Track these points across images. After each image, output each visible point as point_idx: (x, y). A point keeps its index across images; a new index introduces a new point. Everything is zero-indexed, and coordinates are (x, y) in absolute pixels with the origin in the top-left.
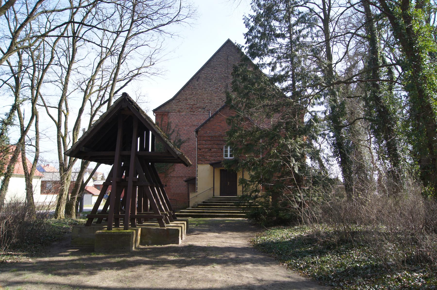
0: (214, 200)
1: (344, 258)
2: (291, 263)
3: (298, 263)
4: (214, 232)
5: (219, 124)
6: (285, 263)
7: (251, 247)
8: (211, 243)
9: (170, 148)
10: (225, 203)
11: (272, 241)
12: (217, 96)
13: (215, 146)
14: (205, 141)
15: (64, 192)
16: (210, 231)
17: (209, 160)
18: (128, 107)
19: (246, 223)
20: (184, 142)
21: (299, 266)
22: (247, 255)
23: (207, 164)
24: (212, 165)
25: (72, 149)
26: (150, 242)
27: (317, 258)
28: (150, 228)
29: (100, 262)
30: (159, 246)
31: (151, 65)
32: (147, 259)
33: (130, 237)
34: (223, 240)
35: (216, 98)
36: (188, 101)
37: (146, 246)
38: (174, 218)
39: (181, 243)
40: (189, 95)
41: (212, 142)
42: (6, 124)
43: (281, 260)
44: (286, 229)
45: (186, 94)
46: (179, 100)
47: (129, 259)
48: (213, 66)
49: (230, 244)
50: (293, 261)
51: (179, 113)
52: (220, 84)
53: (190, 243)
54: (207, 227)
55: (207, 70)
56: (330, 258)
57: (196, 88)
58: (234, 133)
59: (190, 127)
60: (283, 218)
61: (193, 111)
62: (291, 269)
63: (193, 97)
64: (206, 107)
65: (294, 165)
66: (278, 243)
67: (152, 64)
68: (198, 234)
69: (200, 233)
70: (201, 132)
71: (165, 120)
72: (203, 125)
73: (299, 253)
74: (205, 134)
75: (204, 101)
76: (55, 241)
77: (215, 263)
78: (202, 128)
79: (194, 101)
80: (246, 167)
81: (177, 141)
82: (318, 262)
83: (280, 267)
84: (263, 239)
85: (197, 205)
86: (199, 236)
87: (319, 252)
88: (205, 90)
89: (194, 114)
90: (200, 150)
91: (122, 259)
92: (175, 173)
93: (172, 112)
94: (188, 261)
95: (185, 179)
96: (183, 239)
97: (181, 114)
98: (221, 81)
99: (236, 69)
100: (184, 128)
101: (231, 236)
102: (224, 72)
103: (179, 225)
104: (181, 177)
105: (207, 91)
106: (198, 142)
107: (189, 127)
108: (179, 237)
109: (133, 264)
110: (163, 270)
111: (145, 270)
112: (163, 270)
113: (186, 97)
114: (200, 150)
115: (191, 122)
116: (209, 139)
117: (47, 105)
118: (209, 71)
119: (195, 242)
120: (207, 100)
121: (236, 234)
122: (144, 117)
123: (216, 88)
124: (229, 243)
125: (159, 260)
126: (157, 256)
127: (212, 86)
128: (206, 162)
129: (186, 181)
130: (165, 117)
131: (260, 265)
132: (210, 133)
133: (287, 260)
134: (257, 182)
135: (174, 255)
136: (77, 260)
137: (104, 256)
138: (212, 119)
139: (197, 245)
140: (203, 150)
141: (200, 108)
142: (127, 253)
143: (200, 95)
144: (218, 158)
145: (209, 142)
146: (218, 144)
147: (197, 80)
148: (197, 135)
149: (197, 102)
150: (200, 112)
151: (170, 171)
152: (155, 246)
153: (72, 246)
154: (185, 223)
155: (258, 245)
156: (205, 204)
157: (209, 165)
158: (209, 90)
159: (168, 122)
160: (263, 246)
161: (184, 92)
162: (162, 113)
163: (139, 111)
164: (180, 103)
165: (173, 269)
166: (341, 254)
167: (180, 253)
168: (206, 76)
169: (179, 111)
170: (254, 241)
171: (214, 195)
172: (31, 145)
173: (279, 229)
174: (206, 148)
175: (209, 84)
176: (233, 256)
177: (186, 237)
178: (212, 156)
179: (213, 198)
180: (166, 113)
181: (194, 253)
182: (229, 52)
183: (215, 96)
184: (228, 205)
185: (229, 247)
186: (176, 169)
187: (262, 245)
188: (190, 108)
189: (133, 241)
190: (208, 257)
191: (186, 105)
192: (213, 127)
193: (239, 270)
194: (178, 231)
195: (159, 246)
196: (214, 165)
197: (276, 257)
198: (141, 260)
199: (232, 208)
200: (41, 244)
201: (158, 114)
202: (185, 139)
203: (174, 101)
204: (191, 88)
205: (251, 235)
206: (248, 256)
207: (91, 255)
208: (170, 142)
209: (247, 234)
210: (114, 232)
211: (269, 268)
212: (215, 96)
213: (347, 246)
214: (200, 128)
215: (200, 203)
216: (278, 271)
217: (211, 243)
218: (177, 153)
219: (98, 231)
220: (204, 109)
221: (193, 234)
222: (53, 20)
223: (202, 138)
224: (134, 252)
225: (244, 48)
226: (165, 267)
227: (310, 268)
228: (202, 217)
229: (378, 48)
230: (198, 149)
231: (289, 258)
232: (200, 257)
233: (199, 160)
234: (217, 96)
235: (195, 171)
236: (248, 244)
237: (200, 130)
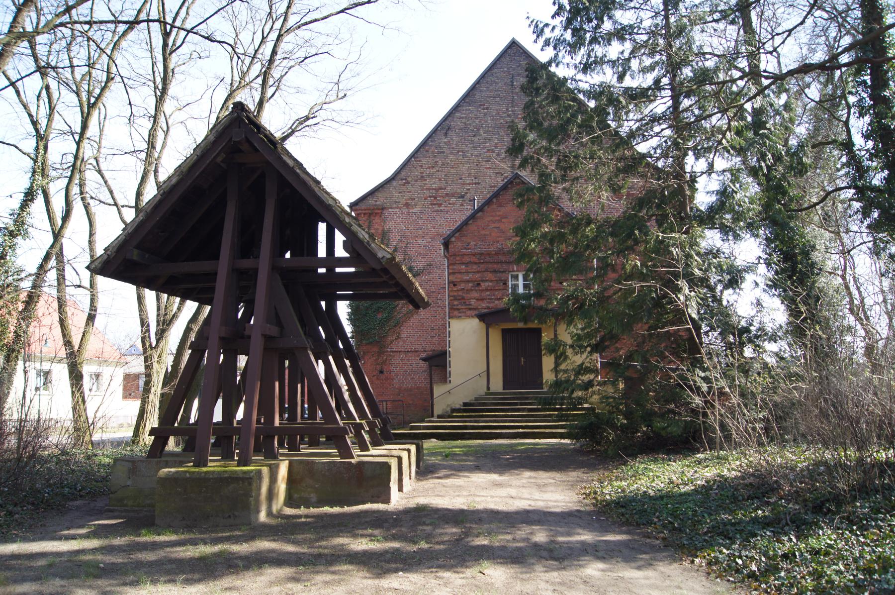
0: (489, 399)
1: (877, 540)
2: (716, 558)
3: (740, 557)
4: (489, 471)
5: (497, 225)
6: (697, 557)
7: (588, 508)
8: (478, 499)
9: (361, 242)
10: (516, 404)
11: (645, 492)
13: (489, 276)
14: (466, 264)
15: (153, 390)
16: (478, 468)
17: (475, 309)
18: (248, 141)
19: (566, 450)
21: (745, 566)
22: (579, 534)
23: (472, 317)
24: (482, 317)
25: (106, 257)
26: (314, 497)
27: (790, 540)
28: (313, 462)
29: (150, 556)
30: (336, 510)
31: (338, 98)
32: (290, 548)
33: (250, 484)
34: (513, 492)
35: (489, 172)
36: (426, 180)
37: (302, 511)
38: (384, 437)
39: (397, 500)
40: (429, 168)
41: (482, 266)
42: (12, 235)
43: (681, 547)
44: (675, 461)
45: (421, 166)
46: (406, 179)
47: (235, 548)
48: (480, 101)
49: (529, 502)
50: (721, 552)
51: (407, 208)
52: (496, 141)
53: (422, 501)
54: (470, 461)
55: (466, 110)
56: (835, 541)
57: (444, 152)
58: (532, 229)
60: (663, 433)
61: (437, 204)
62: (719, 576)
63: (438, 171)
64: (466, 193)
65: (687, 298)
66: (662, 498)
67: (339, 97)
68: (447, 477)
69: (451, 475)
70: (457, 245)
71: (376, 226)
72: (459, 229)
73: (733, 525)
74: (465, 248)
75: (461, 179)
76: (81, 496)
77: (488, 558)
78: (457, 235)
79: (440, 180)
80: (564, 315)
82: (801, 554)
83: (685, 570)
84: (619, 487)
85: (449, 413)
86: (449, 481)
87: (793, 522)
88: (464, 156)
89: (441, 211)
90: (455, 285)
91: (217, 548)
92: (401, 343)
93: (391, 208)
94: (408, 553)
95: (424, 355)
96: (405, 489)
97: (411, 211)
98: (499, 134)
99: (532, 74)
100: (420, 241)
101: (533, 480)
102: (505, 113)
103: (395, 453)
104: (417, 351)
105: (467, 157)
106: (450, 267)
107: (430, 240)
108: (392, 485)
109: (240, 564)
110: (326, 583)
111: (271, 584)
112: (326, 583)
113: (422, 173)
114: (455, 285)
115: (434, 228)
116: (474, 259)
117: (120, 203)
118: (471, 112)
119: (436, 498)
120: (468, 177)
121: (544, 476)
122: (290, 163)
123: (488, 150)
124: (529, 499)
125: (321, 550)
126: (322, 538)
128: (469, 313)
129: (424, 360)
130: (377, 220)
131: (623, 564)
132: (476, 245)
133: (702, 549)
134: (589, 349)
135: (370, 535)
136: (94, 551)
137: (173, 538)
138: (480, 214)
139: (440, 506)
140: (462, 286)
141: (453, 195)
142: (240, 530)
143: (452, 168)
144: (497, 302)
145: (475, 267)
146: (495, 271)
147: (446, 135)
148: (448, 252)
149: (447, 183)
150: (454, 204)
151: (390, 338)
152: (327, 509)
153: (111, 511)
154: (413, 448)
155: (608, 504)
156: (469, 408)
157: (476, 321)
158: (472, 155)
159: (383, 230)
160: (622, 507)
161: (417, 161)
162: (369, 209)
163: (276, 147)
164: (409, 187)
165: (358, 580)
166: (863, 528)
167: (388, 529)
168: (465, 123)
169: (407, 205)
170: (595, 493)
171: (488, 388)
172: (79, 286)
173: (655, 461)
174: (468, 281)
175: (472, 142)
176: (540, 536)
177: (414, 484)
178: (482, 300)
179: (487, 394)
180: (379, 209)
181: (428, 528)
182: (514, 69)
184: (523, 410)
185: (527, 512)
186: (404, 335)
187: (618, 503)
188: (430, 197)
189: (259, 494)
190: (467, 540)
191: (422, 190)
192: (483, 233)
193: (560, 584)
194: (387, 467)
195: (336, 510)
196: (488, 318)
197: (664, 539)
198: (273, 551)
199: (532, 416)
200: (33, 504)
201: (361, 214)
202: (421, 266)
203: (394, 183)
204: (433, 152)
205: (585, 477)
206: (586, 537)
207: (139, 535)
208: (360, 226)
209: (574, 475)
210: (213, 472)
211: (649, 573)
213: (874, 502)
214: (453, 236)
215: (458, 406)
216: (682, 585)
217: (478, 499)
218: (380, 255)
219: (166, 470)
220: (463, 197)
221: (432, 478)
222: (122, 11)
223: (458, 258)
224: (264, 526)
225: (550, 27)
226: (333, 573)
227: (783, 574)
228: (462, 439)
229: (882, 10)
230: (449, 283)
231: (705, 540)
232: (443, 543)
233: (452, 308)
235: (443, 332)
236: (579, 502)
237: (453, 239)
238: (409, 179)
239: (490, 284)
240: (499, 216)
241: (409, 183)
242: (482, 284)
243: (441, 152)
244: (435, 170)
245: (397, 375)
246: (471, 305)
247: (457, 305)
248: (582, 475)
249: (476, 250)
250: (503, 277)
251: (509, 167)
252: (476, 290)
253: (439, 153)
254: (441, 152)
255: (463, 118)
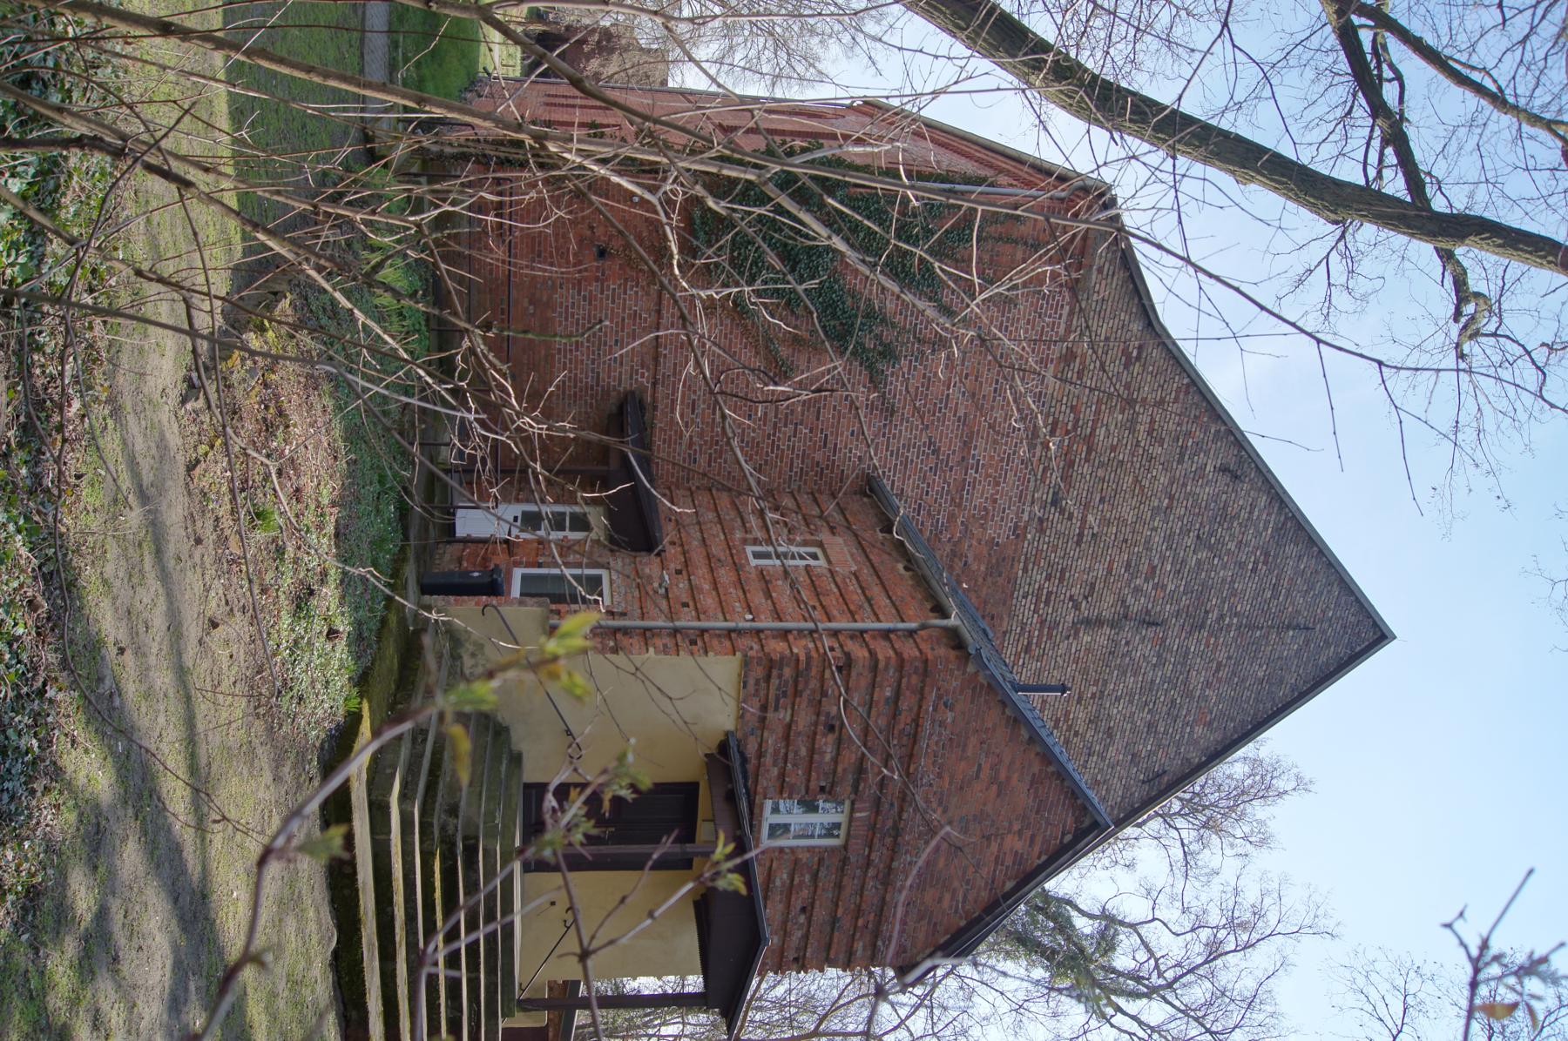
5: (986, 773)
12: (1110, 571)
20: (875, 380)
35: (1100, 570)
40: (1153, 421)
46: (1138, 358)
52: (1171, 587)
55: (1267, 522)
57: (1181, 461)
59: (963, 421)
63: (1138, 445)
64: (1062, 512)
74: (939, 697)
75: (1102, 500)
79: (1113, 448)
81: (888, 335)
88: (1156, 511)
93: (1071, 313)
98: (1185, 593)
102: (1230, 609)
107: (961, 413)
116: (905, 719)
120: (1103, 519)
127: (1169, 548)
128: (753, 709)
132: (942, 724)
144: (775, 771)
147: (1224, 469)
149: (1101, 465)
161: (1178, 390)
168: (1237, 517)
175: (1186, 531)
178: (787, 738)
182: (1324, 632)
183: (1111, 562)
188: (1077, 420)
192: (973, 740)
202: (896, 385)
203: (1136, 326)
212: (1111, 562)
220: (1055, 503)
223: (915, 680)
233: (771, 665)
234: (1110, 571)
238: (1137, 368)
239: (828, 757)
240: (1008, 778)
241: (1126, 366)
242: (831, 738)
243: (1182, 455)
244: (1142, 436)
245: (590, 299)
246: (776, 709)
247: (780, 676)
248: (264, 1027)
249: (927, 725)
250: (844, 789)
251: (1100, 614)
252: (816, 724)
253: (1183, 448)
254: (1182, 455)
255: (1251, 513)
